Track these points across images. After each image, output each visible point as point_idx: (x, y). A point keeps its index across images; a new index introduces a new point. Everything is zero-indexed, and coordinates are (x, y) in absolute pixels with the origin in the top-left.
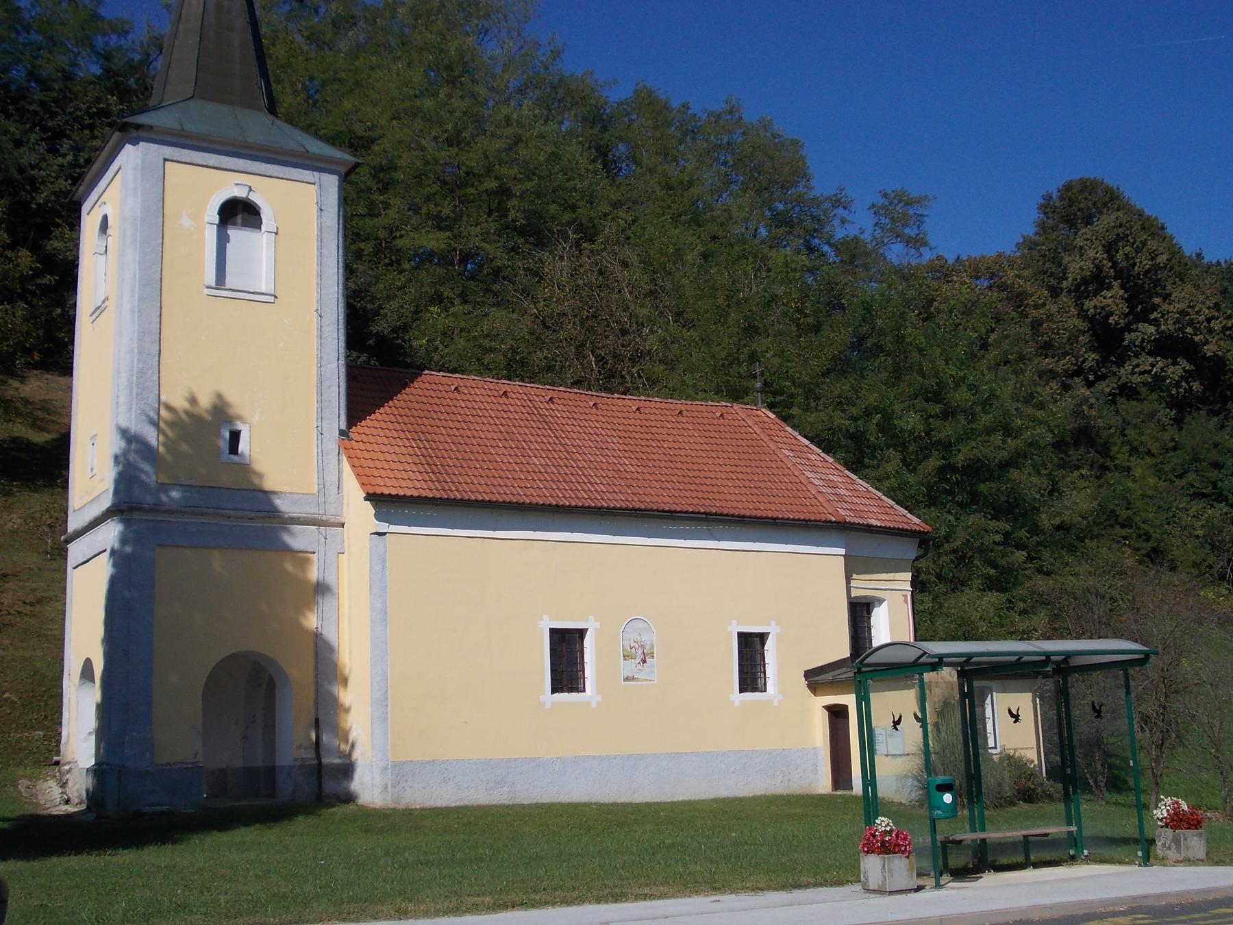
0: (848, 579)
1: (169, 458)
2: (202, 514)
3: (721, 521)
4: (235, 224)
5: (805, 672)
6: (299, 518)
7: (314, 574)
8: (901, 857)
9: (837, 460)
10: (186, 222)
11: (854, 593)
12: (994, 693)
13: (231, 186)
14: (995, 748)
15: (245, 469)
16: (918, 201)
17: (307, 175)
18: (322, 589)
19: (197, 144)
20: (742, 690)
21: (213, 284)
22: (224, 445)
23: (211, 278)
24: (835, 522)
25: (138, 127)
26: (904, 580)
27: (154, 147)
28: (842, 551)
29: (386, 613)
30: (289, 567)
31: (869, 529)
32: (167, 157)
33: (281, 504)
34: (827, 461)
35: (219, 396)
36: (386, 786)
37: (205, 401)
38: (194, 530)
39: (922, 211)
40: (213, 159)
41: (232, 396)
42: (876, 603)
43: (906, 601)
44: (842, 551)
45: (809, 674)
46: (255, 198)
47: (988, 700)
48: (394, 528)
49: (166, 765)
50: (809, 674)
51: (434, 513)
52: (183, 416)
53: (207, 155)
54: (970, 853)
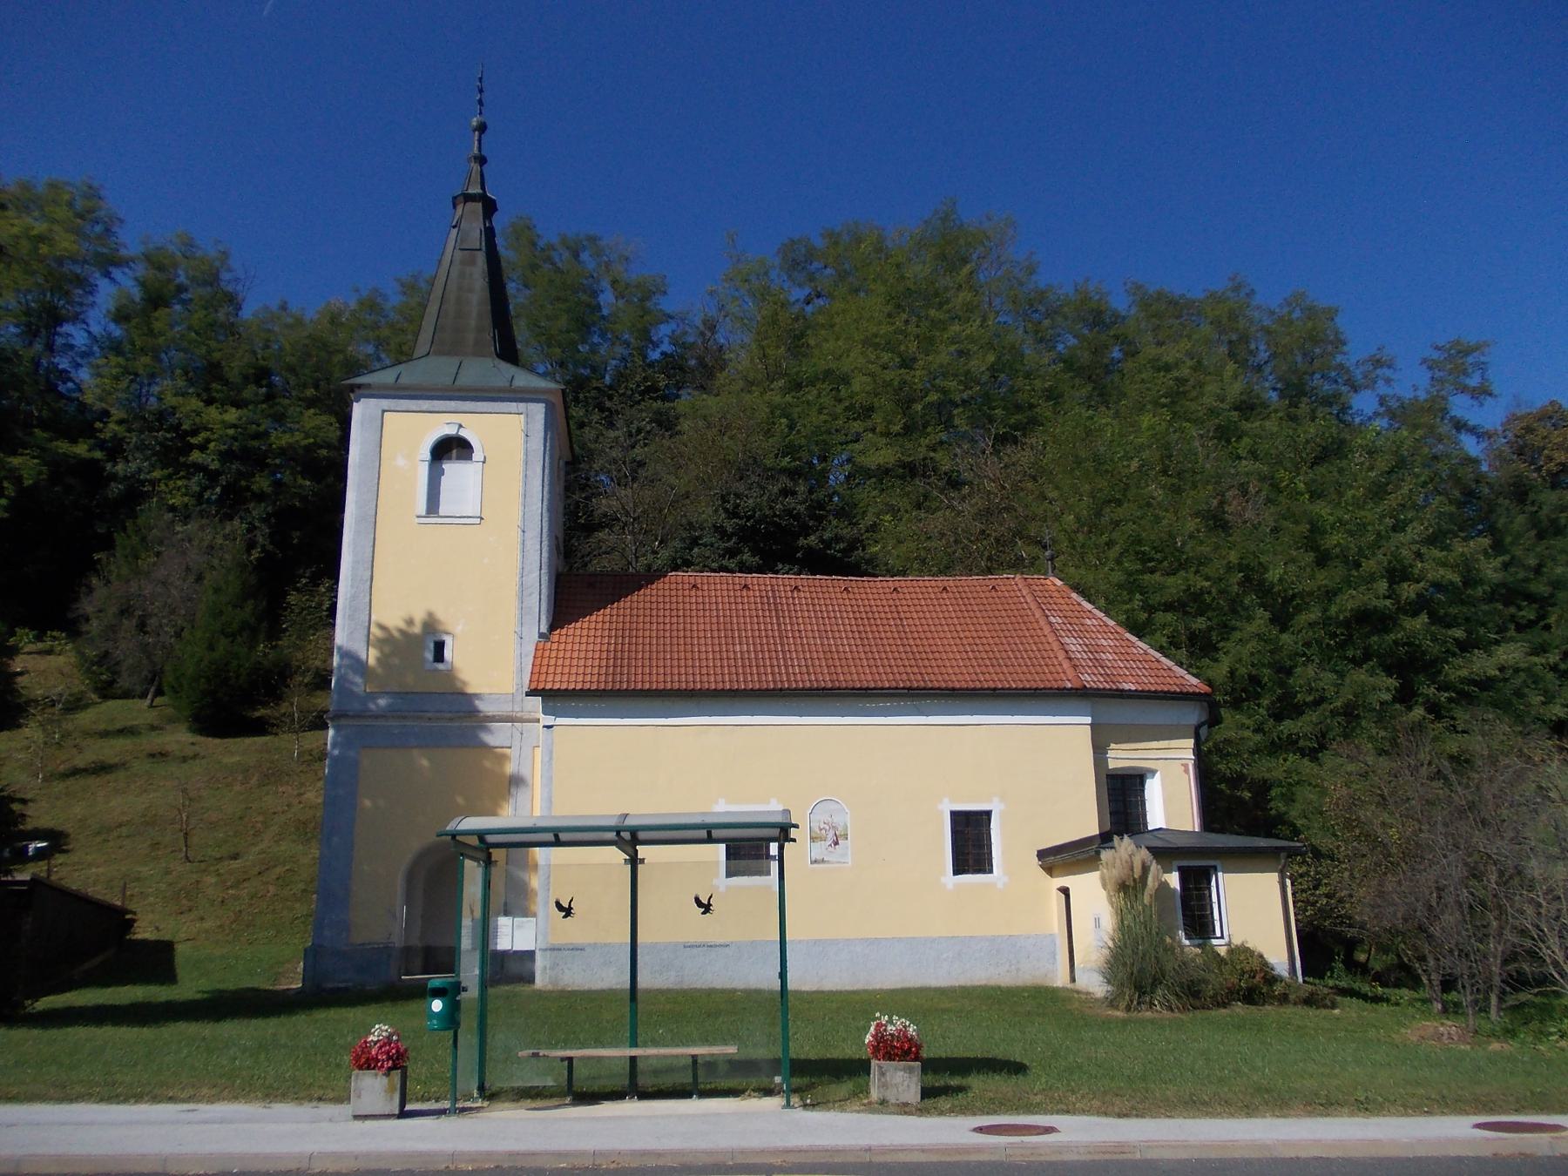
0: (1099, 750)
1: (379, 670)
2: (405, 718)
3: (942, 695)
4: (450, 459)
5: (1039, 852)
6: (494, 716)
7: (510, 768)
8: (376, 1075)
9: (1119, 623)
10: (401, 462)
11: (1112, 765)
12: (1220, 874)
13: (440, 424)
14: (1222, 937)
15: (450, 675)
16: (1477, 348)
17: (513, 406)
18: (516, 781)
19: (413, 393)
20: (957, 872)
21: (424, 513)
22: (430, 656)
23: (422, 507)
24: (1071, 689)
25: (359, 386)
26: (1184, 749)
27: (373, 401)
28: (1088, 720)
29: (551, 802)
30: (488, 764)
31: (1121, 695)
32: (386, 408)
33: (485, 707)
34: (1107, 626)
35: (430, 615)
36: (545, 967)
37: (419, 617)
38: (396, 732)
39: (1483, 359)
40: (426, 404)
41: (441, 615)
42: (1148, 775)
43: (1186, 771)
44: (1088, 720)
45: (1041, 854)
46: (463, 433)
47: (1213, 883)
48: (560, 721)
49: (360, 945)
50: (1041, 854)
51: (657, 704)
52: (396, 634)
53: (420, 402)
54: (356, 1071)
